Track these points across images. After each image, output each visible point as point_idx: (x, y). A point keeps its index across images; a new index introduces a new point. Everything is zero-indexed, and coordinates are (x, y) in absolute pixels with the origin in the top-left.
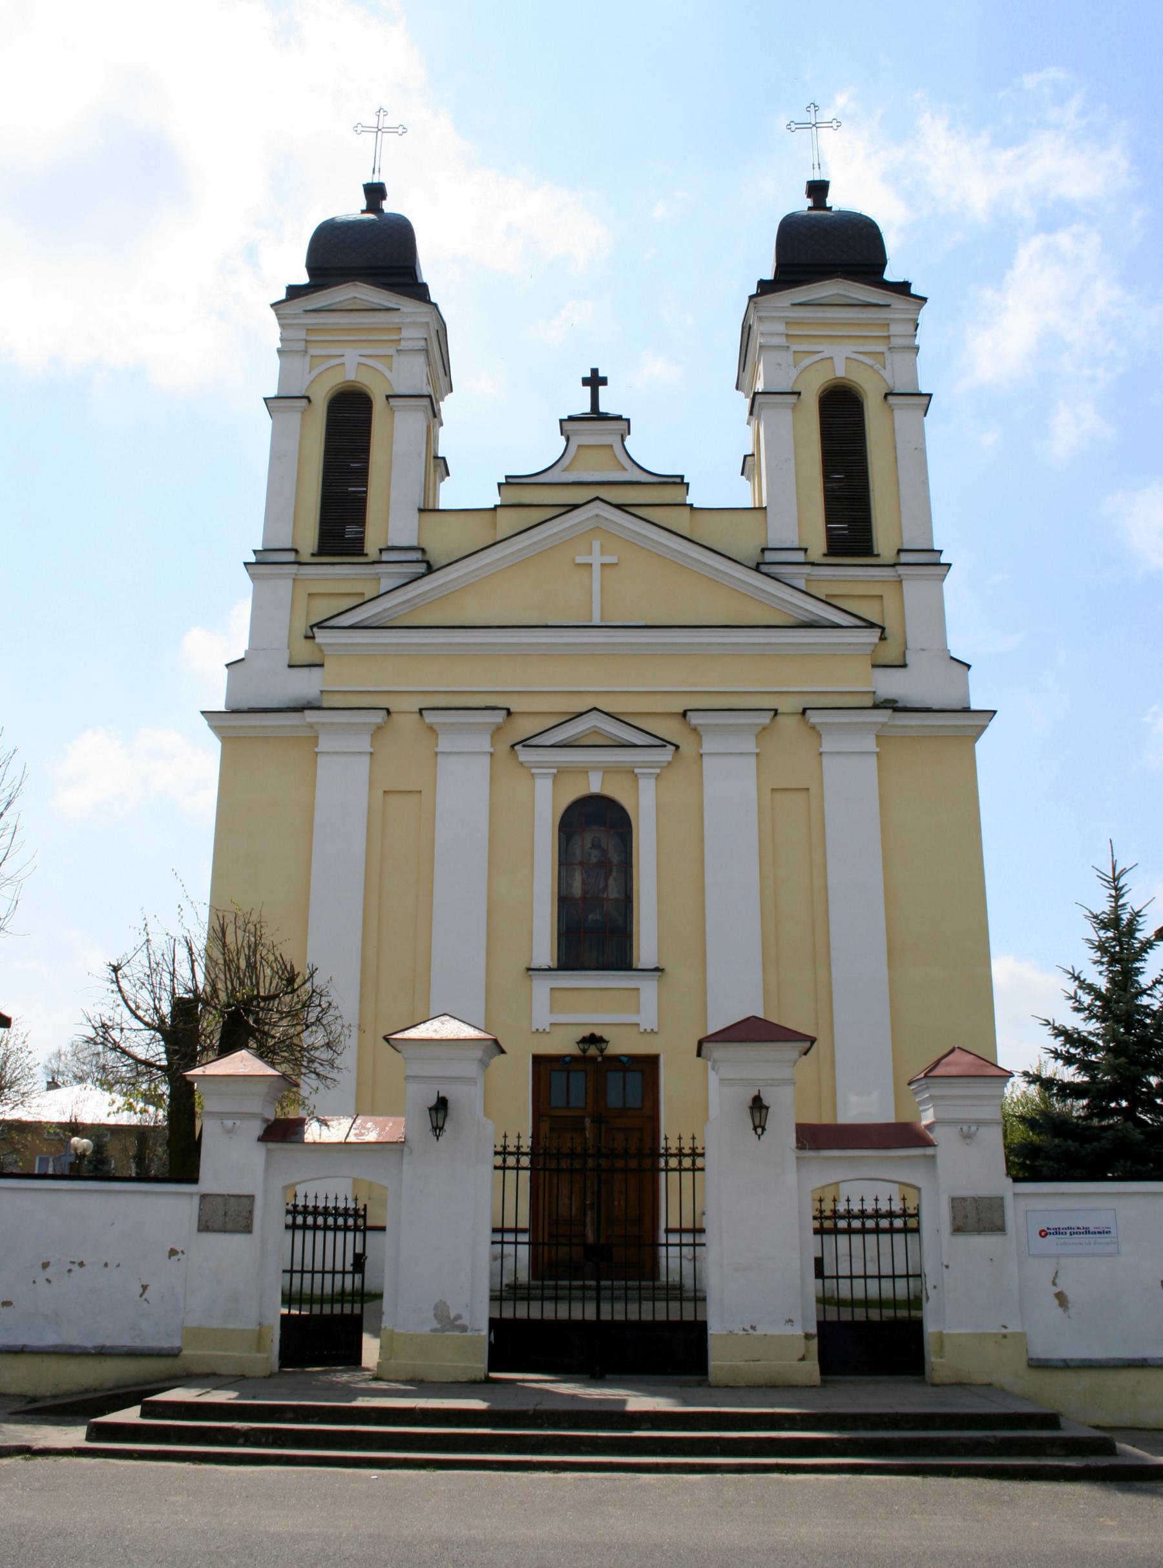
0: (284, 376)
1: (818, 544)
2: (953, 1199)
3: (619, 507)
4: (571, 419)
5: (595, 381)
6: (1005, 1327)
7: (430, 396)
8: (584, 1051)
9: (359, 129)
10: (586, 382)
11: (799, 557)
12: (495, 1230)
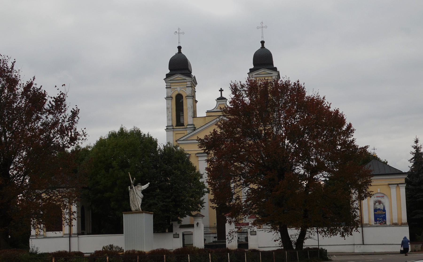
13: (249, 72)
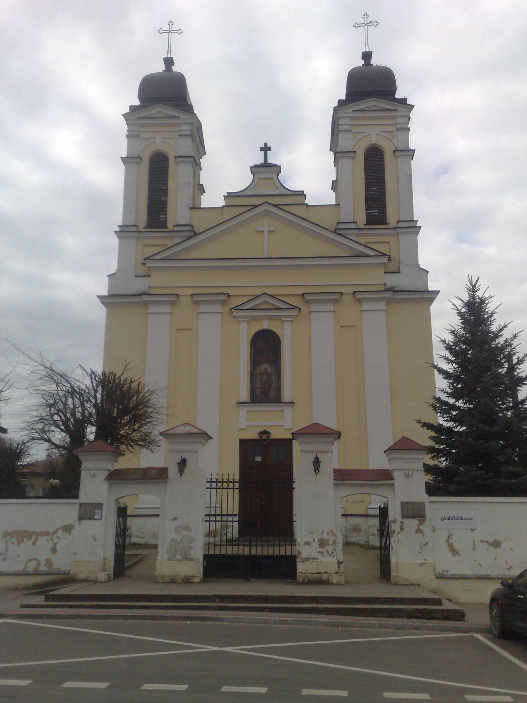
0: (130, 148)
1: (362, 219)
2: (402, 503)
3: (275, 206)
4: (256, 166)
5: (266, 149)
6: (425, 560)
7: (193, 157)
8: (261, 437)
9: (161, 31)
10: (262, 149)
11: (353, 226)
12: (207, 515)
13: (343, 97)
